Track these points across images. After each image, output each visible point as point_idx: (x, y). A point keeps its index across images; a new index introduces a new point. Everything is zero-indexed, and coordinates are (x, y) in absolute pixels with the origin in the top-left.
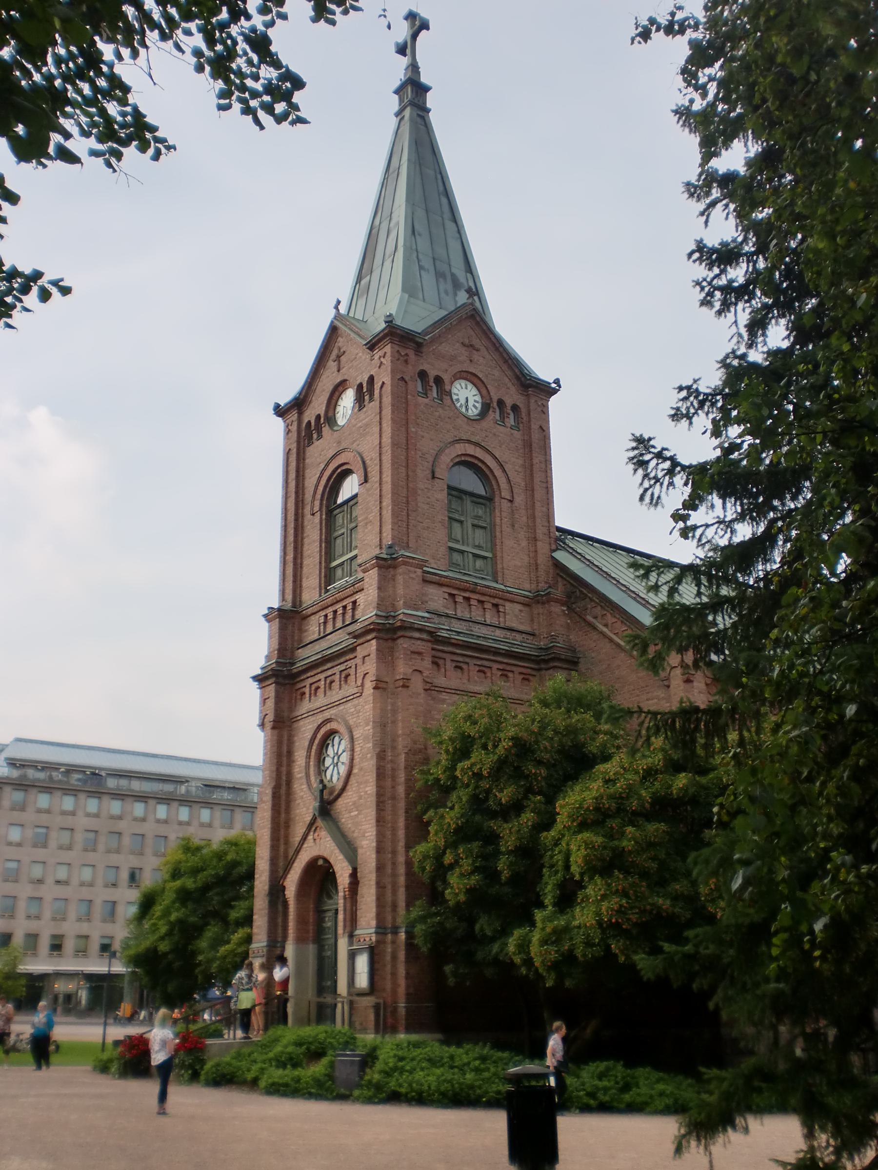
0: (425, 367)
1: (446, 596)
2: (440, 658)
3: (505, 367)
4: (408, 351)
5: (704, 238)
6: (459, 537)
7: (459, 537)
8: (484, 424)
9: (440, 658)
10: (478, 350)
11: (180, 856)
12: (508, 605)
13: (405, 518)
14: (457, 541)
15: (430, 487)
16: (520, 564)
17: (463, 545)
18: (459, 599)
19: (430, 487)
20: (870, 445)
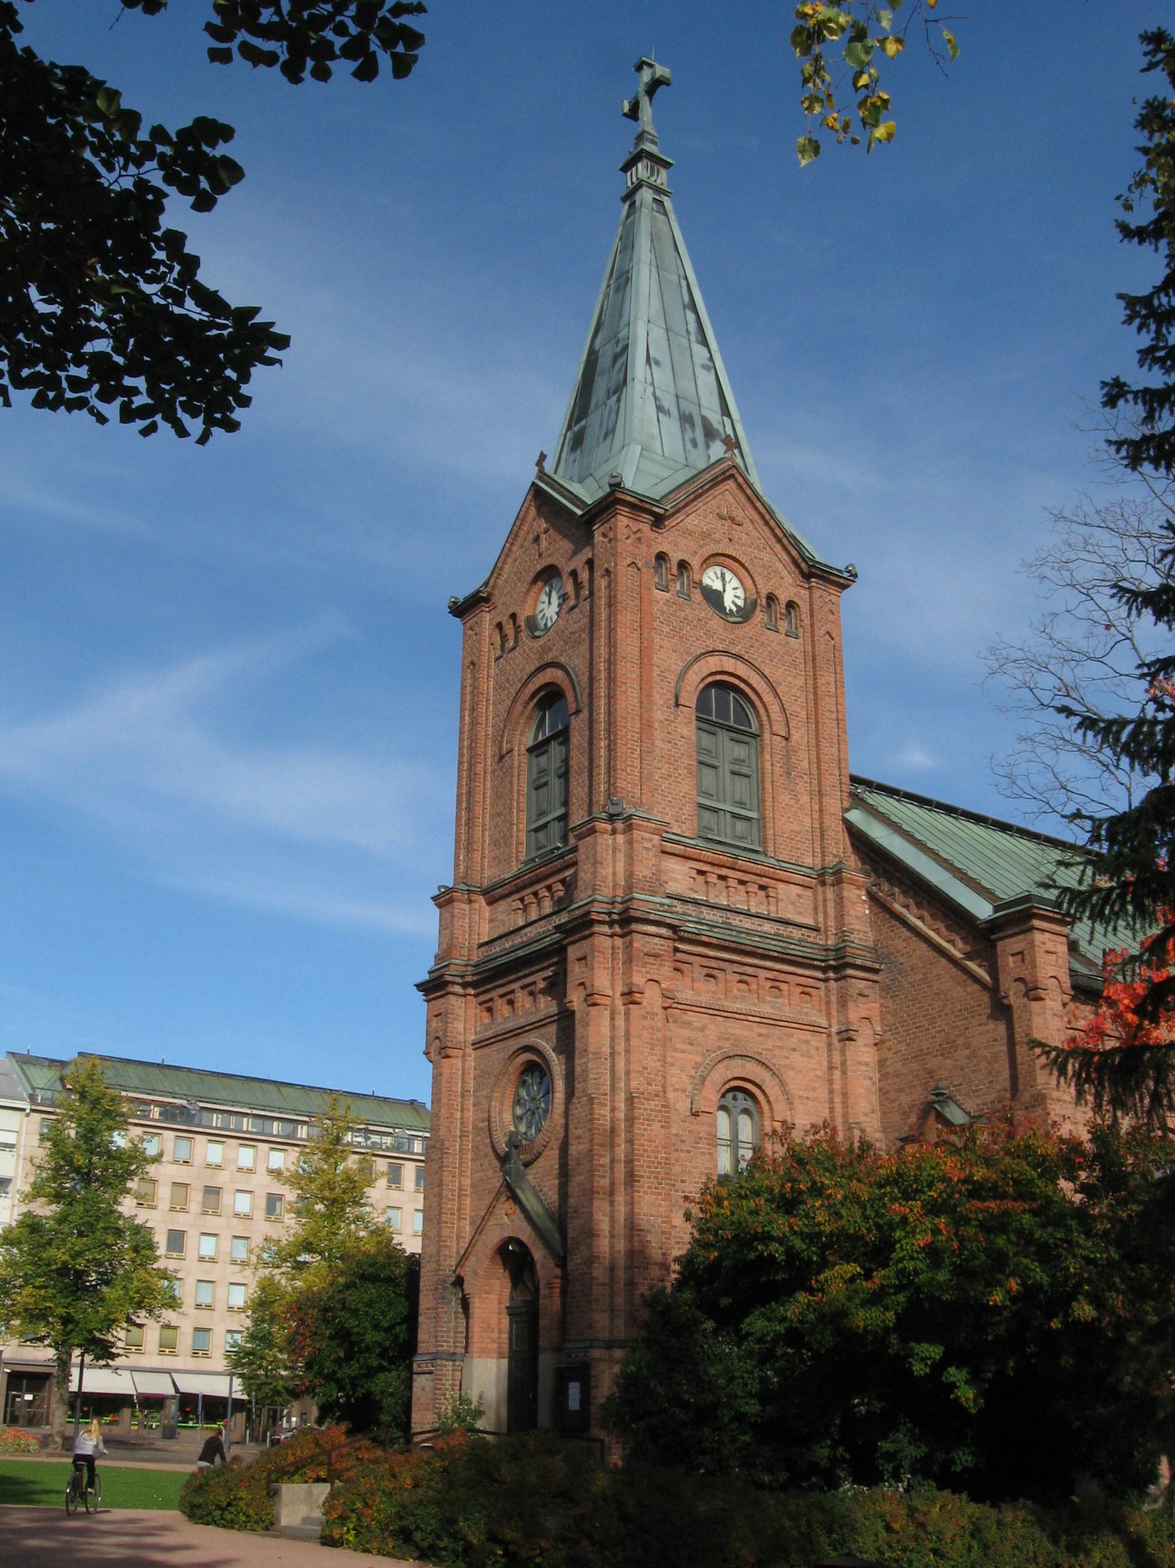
12: (781, 886)
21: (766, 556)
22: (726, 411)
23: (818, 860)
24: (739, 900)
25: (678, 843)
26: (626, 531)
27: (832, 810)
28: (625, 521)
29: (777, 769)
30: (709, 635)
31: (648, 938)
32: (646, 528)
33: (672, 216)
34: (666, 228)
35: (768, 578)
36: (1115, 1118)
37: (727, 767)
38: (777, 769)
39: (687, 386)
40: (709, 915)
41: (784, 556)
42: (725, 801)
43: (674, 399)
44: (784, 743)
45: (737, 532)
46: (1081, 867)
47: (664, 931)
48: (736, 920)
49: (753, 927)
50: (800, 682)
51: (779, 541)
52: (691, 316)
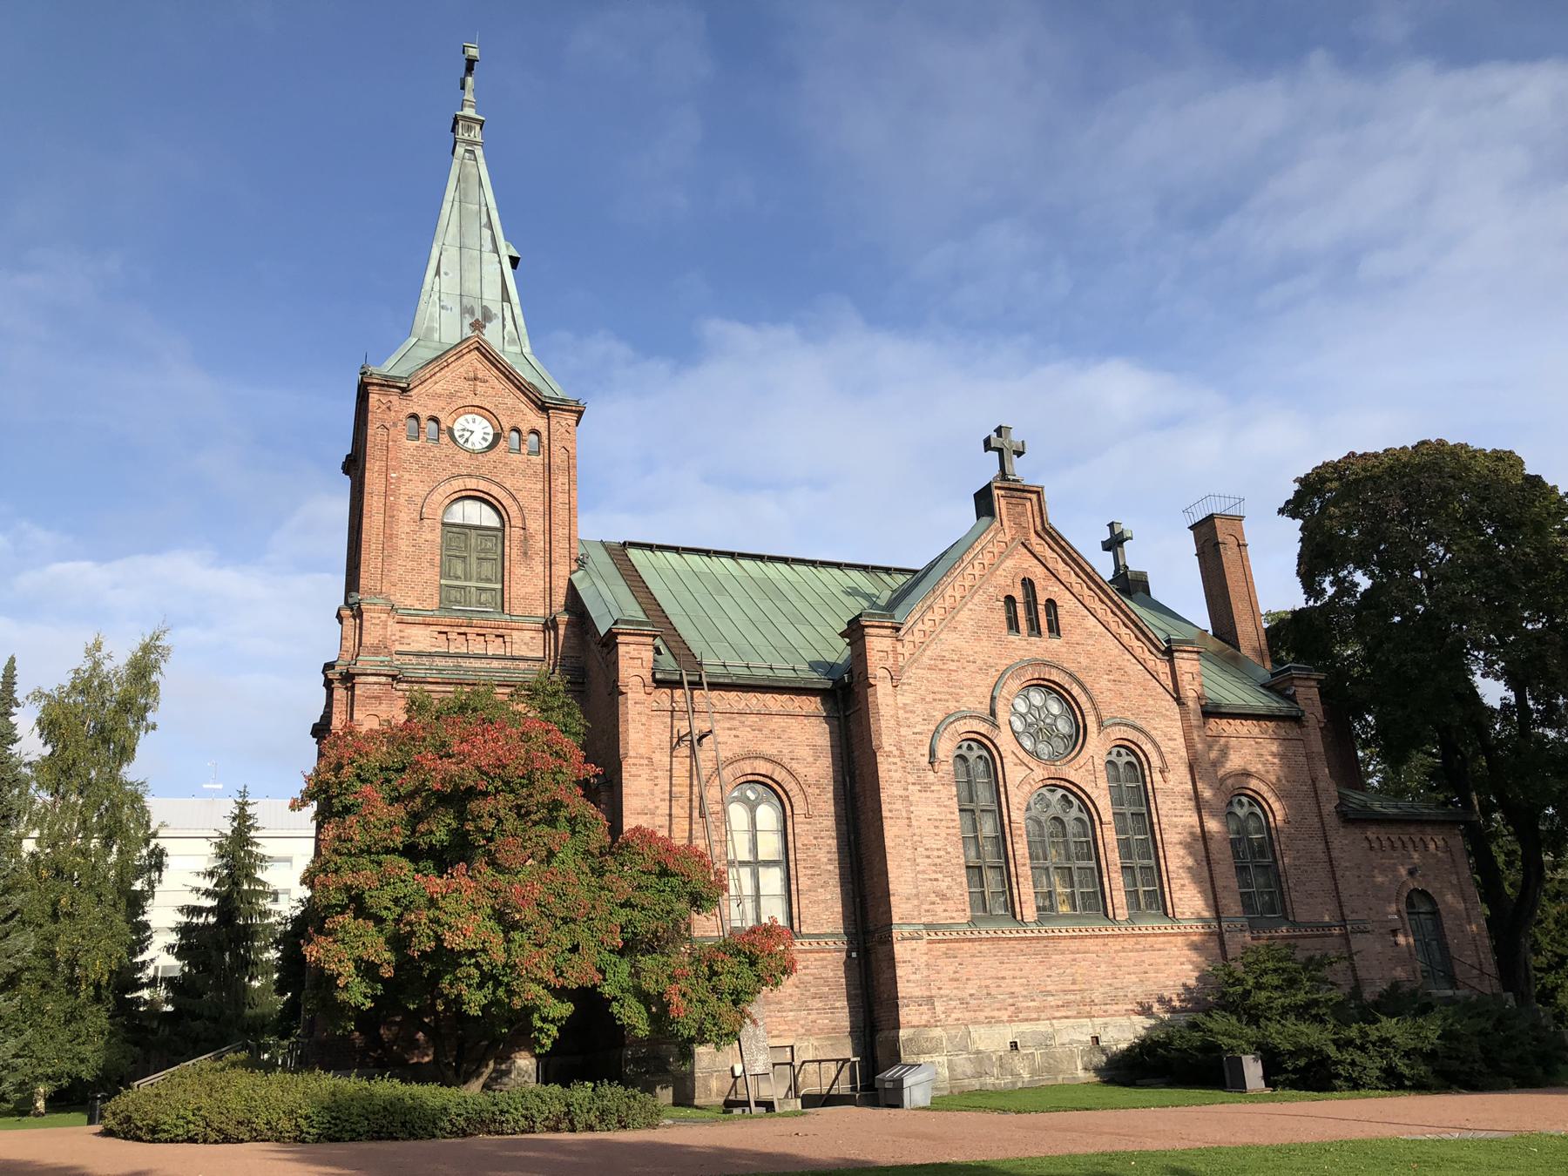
0: (416, 410)
1: (436, 634)
2: (1026, 498)
3: (519, 394)
4: (391, 398)
5: (172, 658)
6: (459, 573)
7: (459, 573)
8: (492, 455)
9: (1026, 498)
10: (485, 381)
11: (1377, 998)
12: (515, 633)
13: (380, 565)
14: (457, 578)
15: (417, 529)
16: (532, 591)
17: (466, 580)
18: (452, 636)
19: (417, 529)
20: (3, 823)
21: (510, 401)
22: (505, 296)
23: (548, 611)
24: (477, 647)
25: (417, 615)
26: (377, 404)
27: (561, 573)
28: (377, 397)
29: (515, 551)
31: (368, 686)
32: (394, 399)
33: (481, 161)
34: (474, 171)
35: (512, 416)
36: (153, 983)
37: (474, 555)
38: (515, 551)
39: (472, 286)
40: (440, 662)
41: (524, 398)
42: (470, 580)
43: (459, 298)
44: (522, 531)
45: (480, 387)
46: (340, 662)
47: (383, 679)
48: (465, 663)
49: (482, 666)
50: (540, 486)
51: (519, 389)
52: (487, 233)
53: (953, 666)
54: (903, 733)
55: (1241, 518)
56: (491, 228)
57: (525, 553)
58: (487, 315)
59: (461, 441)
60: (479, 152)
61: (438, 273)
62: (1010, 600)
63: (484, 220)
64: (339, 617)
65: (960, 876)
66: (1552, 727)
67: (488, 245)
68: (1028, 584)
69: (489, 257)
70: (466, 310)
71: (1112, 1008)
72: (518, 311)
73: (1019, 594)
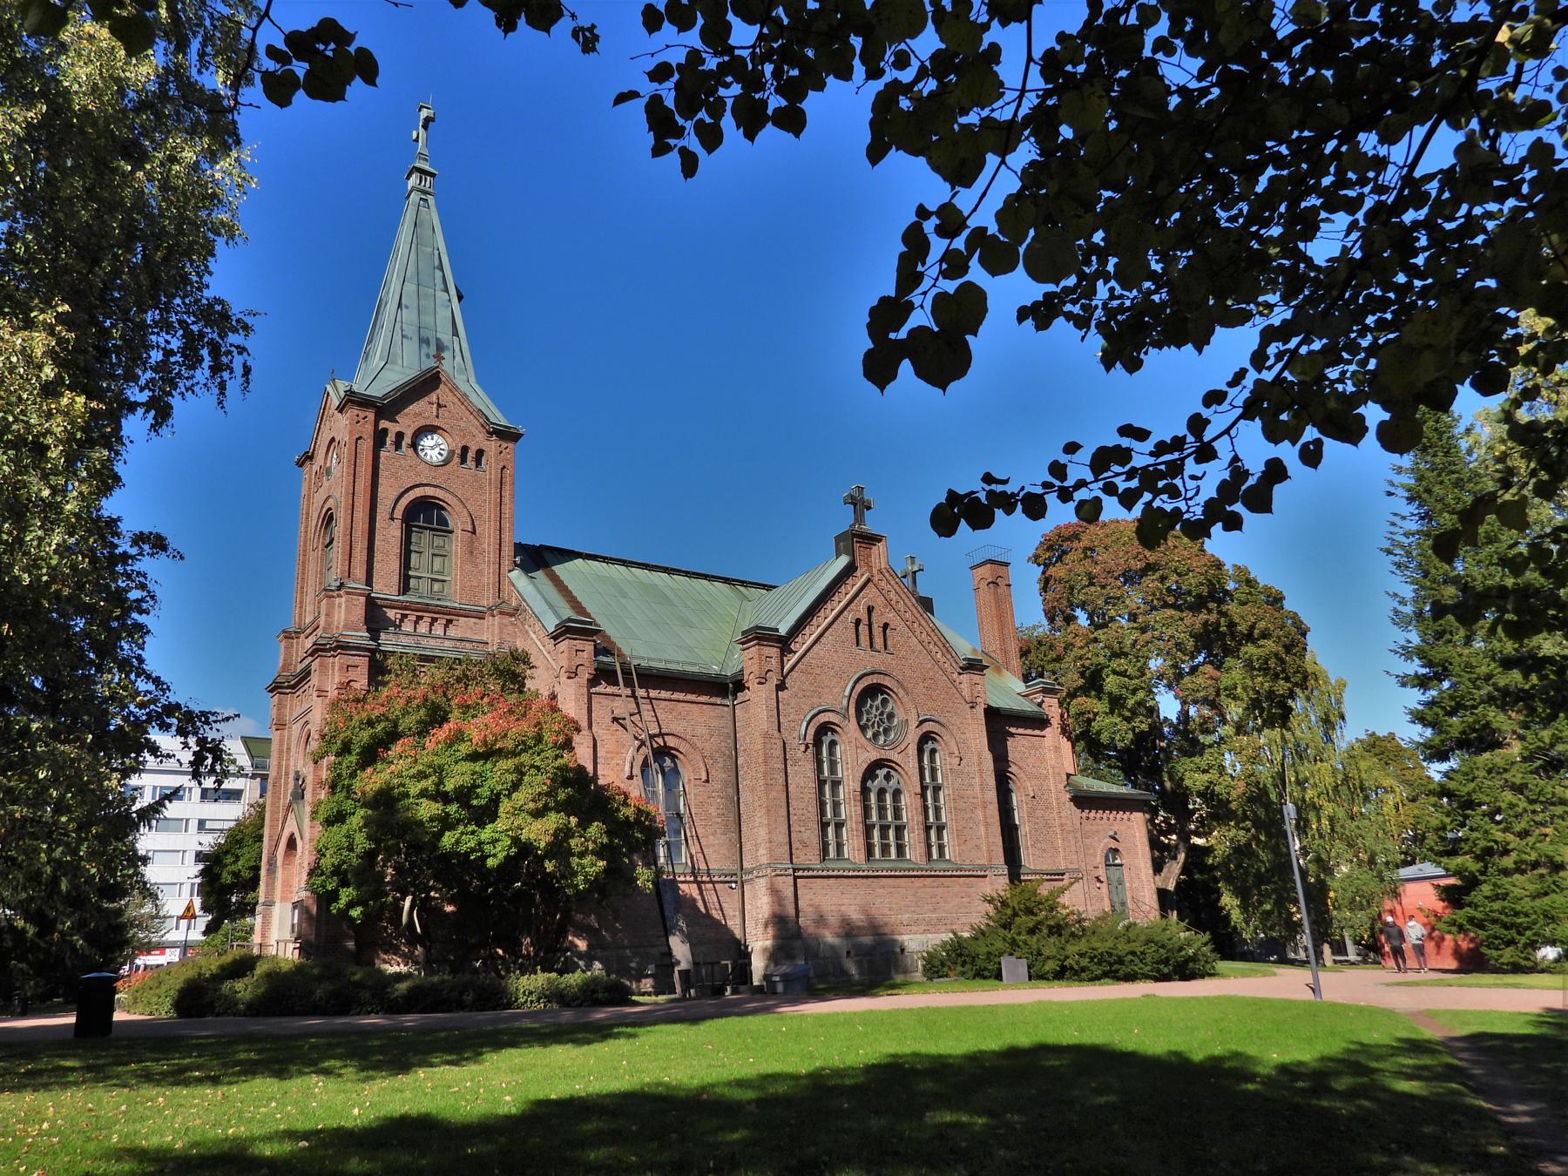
8: (441, 470)
22: (455, 333)
30: (417, 474)
33: (433, 208)
39: (427, 319)
53: (818, 671)
54: (115, 775)
55: (1007, 564)
56: (442, 270)
57: (472, 553)
58: (440, 347)
59: (422, 454)
60: (431, 199)
61: (400, 305)
62: (858, 622)
63: (437, 263)
64: (1342, 717)
65: (214, 1095)
66: (128, 162)
67: (440, 285)
68: (870, 610)
69: (441, 295)
70: (424, 341)
71: (914, 928)
72: (465, 345)
73: (864, 618)
